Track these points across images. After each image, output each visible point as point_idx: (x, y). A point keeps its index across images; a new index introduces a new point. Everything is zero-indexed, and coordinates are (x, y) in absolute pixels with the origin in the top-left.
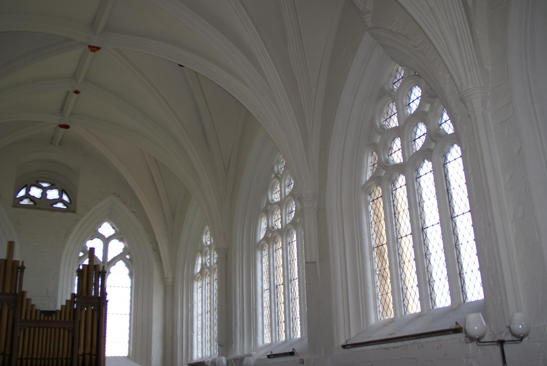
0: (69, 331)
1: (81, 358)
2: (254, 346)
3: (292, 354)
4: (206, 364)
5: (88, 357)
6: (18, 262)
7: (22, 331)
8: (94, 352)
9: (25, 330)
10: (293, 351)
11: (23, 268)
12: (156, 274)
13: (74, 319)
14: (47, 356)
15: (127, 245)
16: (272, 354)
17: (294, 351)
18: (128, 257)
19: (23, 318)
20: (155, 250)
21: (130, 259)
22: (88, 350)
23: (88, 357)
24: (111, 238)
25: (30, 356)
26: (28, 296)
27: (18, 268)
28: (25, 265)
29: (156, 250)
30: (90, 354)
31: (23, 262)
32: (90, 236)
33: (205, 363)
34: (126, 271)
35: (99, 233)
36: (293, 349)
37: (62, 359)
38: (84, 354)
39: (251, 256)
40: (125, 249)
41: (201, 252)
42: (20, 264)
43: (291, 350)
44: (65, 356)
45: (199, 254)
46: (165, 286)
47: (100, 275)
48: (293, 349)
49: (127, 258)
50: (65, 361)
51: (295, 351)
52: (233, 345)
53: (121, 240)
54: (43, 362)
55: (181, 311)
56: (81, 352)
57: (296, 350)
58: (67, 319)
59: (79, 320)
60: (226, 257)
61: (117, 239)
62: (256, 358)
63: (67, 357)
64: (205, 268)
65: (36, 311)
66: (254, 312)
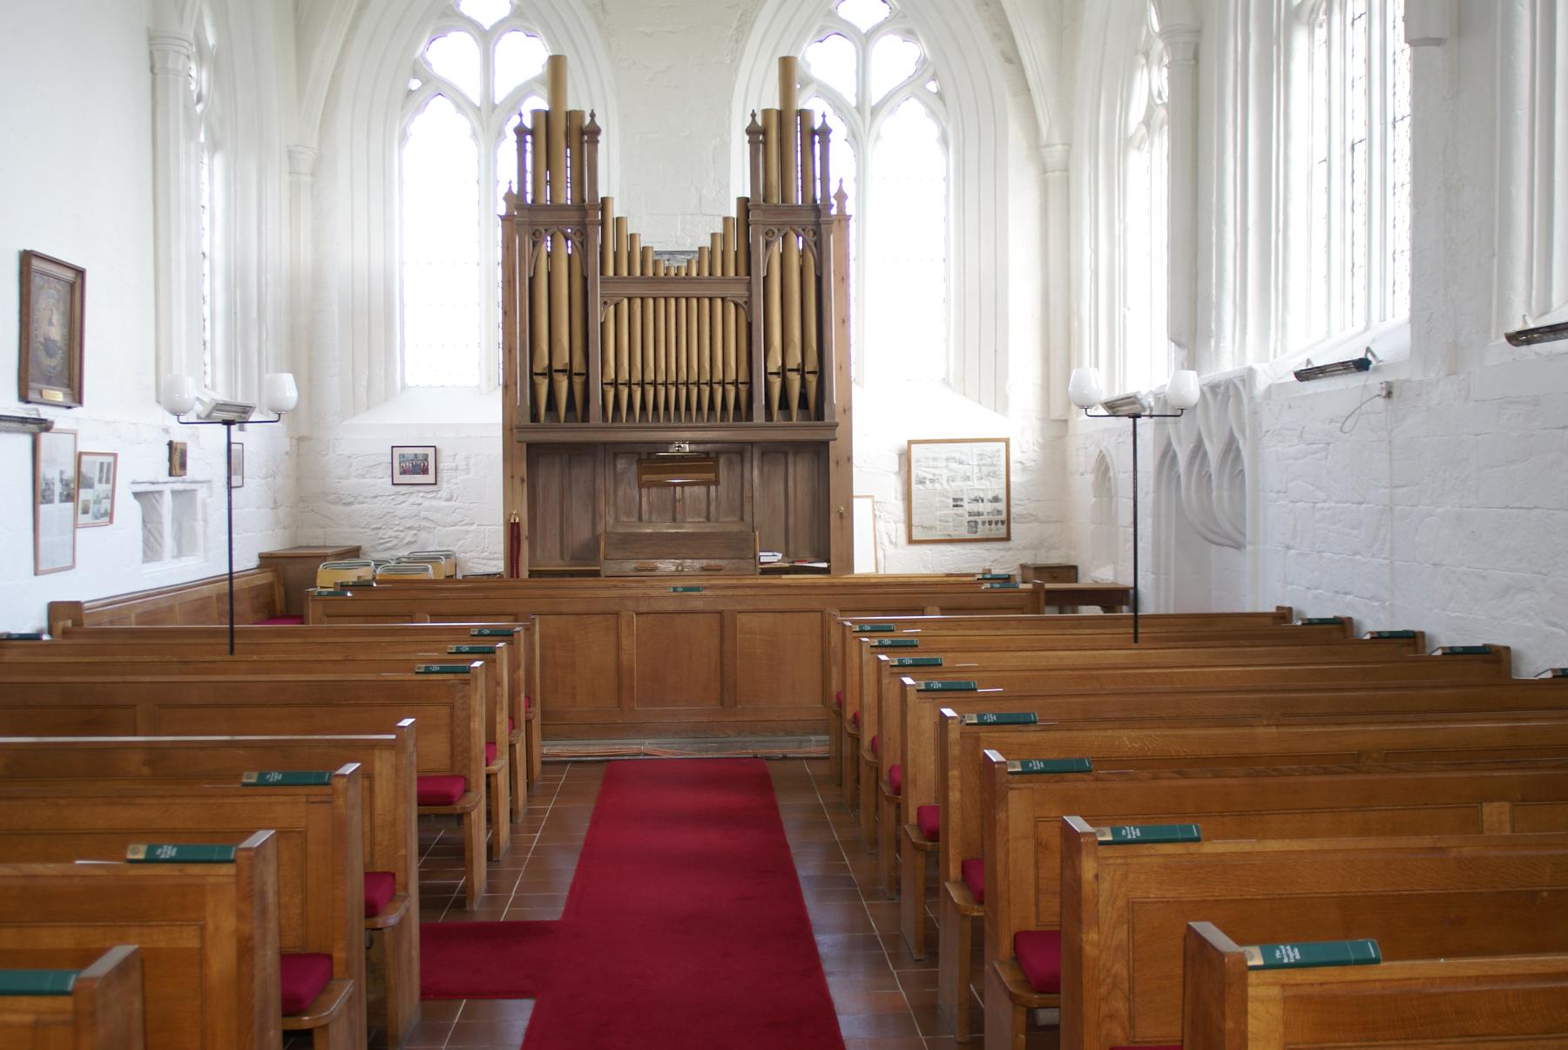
0: (737, 305)
1: (776, 383)
2: (1279, 345)
3: (1362, 365)
4: (1143, 401)
5: (795, 379)
6: (580, 114)
7: (612, 308)
8: (812, 364)
9: (617, 306)
10: (1366, 355)
11: (594, 132)
12: (1015, 134)
13: (749, 273)
14: (683, 377)
15: (806, 45)
16: (1310, 367)
17: (1370, 357)
18: (933, 87)
19: (611, 273)
20: (1009, 60)
21: (940, 95)
22: (795, 359)
23: (795, 379)
24: (875, 31)
25: (637, 377)
26: (616, 211)
27: (582, 132)
28: (599, 121)
29: (1012, 58)
30: (801, 370)
31: (593, 115)
32: (812, 33)
33: (1139, 397)
34: (931, 130)
35: (839, 17)
36: (1368, 350)
37: (615, 384)
38: (783, 372)
39: (1275, 48)
40: (923, 62)
41: (1147, 55)
42: (587, 120)
43: (1359, 354)
44: (732, 376)
45: (1143, 61)
46: (1044, 170)
47: (817, 138)
48: (1368, 350)
49: (930, 92)
50: (731, 390)
51: (1374, 355)
52: (1213, 344)
53: (909, 34)
54: (673, 391)
55: (1093, 246)
56: (775, 363)
57: (1376, 353)
58: (732, 273)
59: (762, 274)
60: (1196, 57)
61: (894, 32)
62: (1270, 381)
63: (737, 379)
64: (1157, 105)
65: (644, 251)
66: (1281, 234)
